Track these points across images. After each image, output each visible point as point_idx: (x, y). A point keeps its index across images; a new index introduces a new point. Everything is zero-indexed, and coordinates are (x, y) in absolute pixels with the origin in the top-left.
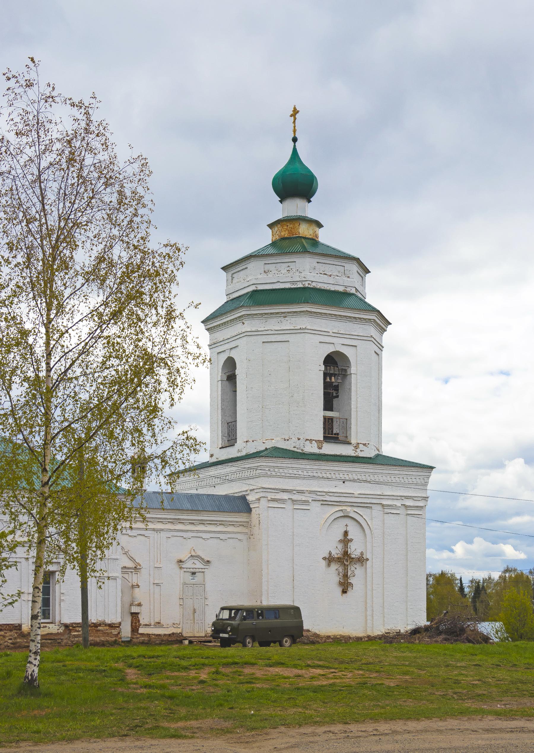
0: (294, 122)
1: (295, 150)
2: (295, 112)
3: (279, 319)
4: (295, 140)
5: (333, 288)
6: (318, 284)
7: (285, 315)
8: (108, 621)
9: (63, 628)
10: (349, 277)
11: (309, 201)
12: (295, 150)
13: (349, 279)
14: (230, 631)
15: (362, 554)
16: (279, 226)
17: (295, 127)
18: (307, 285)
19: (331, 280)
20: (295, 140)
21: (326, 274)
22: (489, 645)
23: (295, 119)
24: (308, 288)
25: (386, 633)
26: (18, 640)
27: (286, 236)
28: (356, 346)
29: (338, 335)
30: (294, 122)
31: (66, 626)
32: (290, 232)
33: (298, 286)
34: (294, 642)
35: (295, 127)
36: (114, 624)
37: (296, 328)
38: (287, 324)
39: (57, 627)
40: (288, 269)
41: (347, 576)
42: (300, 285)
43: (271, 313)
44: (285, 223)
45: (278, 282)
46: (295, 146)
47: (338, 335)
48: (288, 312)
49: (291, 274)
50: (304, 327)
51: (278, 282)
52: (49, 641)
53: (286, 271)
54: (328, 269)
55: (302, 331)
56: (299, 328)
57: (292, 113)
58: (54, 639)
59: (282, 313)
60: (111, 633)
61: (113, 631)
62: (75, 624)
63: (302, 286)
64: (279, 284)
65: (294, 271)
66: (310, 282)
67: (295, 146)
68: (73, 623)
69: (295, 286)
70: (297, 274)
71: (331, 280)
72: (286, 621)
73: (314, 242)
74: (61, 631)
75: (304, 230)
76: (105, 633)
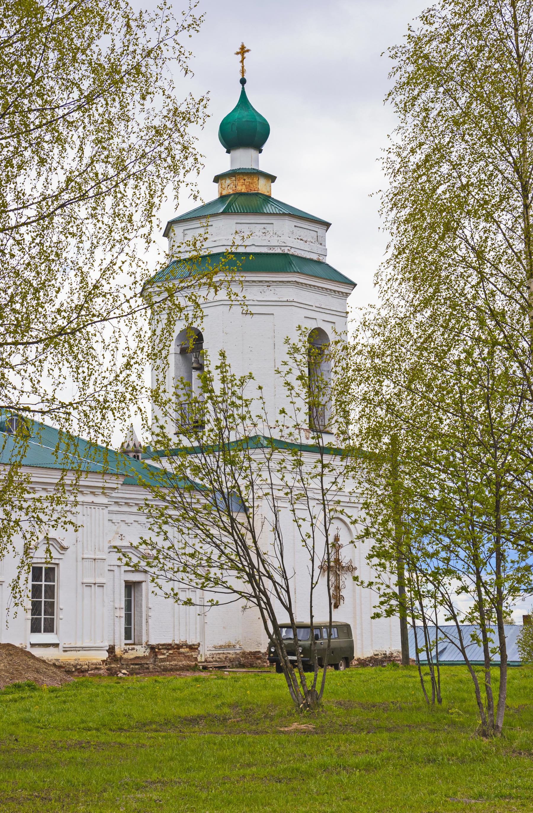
0: (242, 62)
1: (243, 93)
2: (243, 51)
3: (262, 288)
4: (243, 82)
5: (308, 256)
6: (296, 250)
7: (269, 284)
8: (190, 643)
9: (149, 650)
10: (321, 244)
11: (260, 151)
12: (243, 93)
13: (320, 246)
14: (301, 653)
15: (351, 561)
16: (234, 178)
17: (243, 67)
18: (286, 252)
19: (306, 247)
20: (243, 82)
21: (301, 240)
22: (353, 671)
23: (243, 58)
24: (288, 254)
25: (375, 655)
26: (113, 666)
27: (243, 191)
28: (334, 323)
29: (320, 309)
30: (242, 62)
31: (152, 648)
32: (248, 187)
33: (276, 252)
34: (347, 665)
35: (243, 67)
36: (194, 645)
37: (281, 300)
38: (270, 295)
39: (143, 649)
40: (264, 231)
41: (339, 587)
42: (278, 251)
43: (253, 281)
44: (241, 176)
45: (253, 245)
46: (243, 88)
47: (320, 309)
48: (273, 281)
49: (268, 237)
50: (291, 300)
51: (253, 245)
52: (137, 667)
53: (261, 234)
54: (304, 234)
55: (289, 303)
56: (285, 299)
57: (239, 51)
58: (141, 664)
59: (266, 281)
60: (192, 655)
61: (193, 653)
62: (161, 645)
63: (281, 252)
64: (253, 247)
65: (271, 234)
66: (289, 248)
67: (243, 88)
68: (158, 645)
69: (273, 252)
70: (276, 237)
71: (306, 247)
72: (337, 641)
73: (267, 199)
74: (147, 654)
75: (262, 186)
76: (186, 656)
